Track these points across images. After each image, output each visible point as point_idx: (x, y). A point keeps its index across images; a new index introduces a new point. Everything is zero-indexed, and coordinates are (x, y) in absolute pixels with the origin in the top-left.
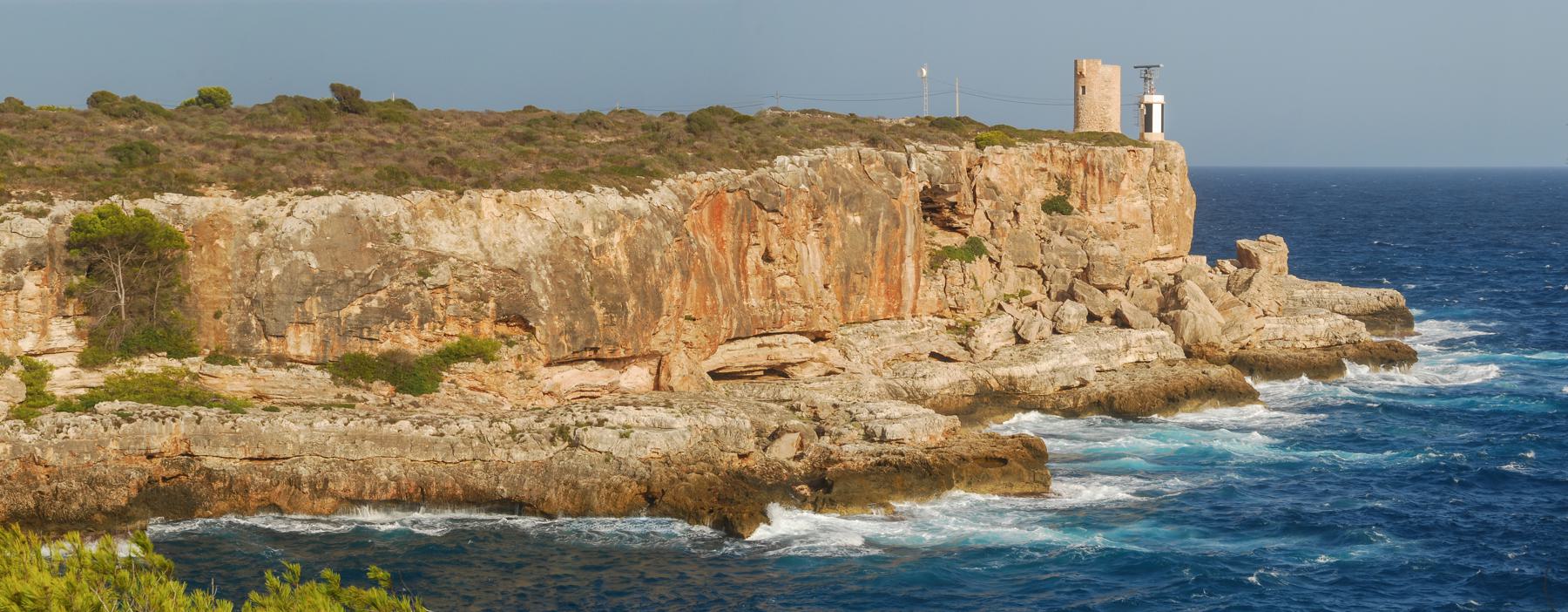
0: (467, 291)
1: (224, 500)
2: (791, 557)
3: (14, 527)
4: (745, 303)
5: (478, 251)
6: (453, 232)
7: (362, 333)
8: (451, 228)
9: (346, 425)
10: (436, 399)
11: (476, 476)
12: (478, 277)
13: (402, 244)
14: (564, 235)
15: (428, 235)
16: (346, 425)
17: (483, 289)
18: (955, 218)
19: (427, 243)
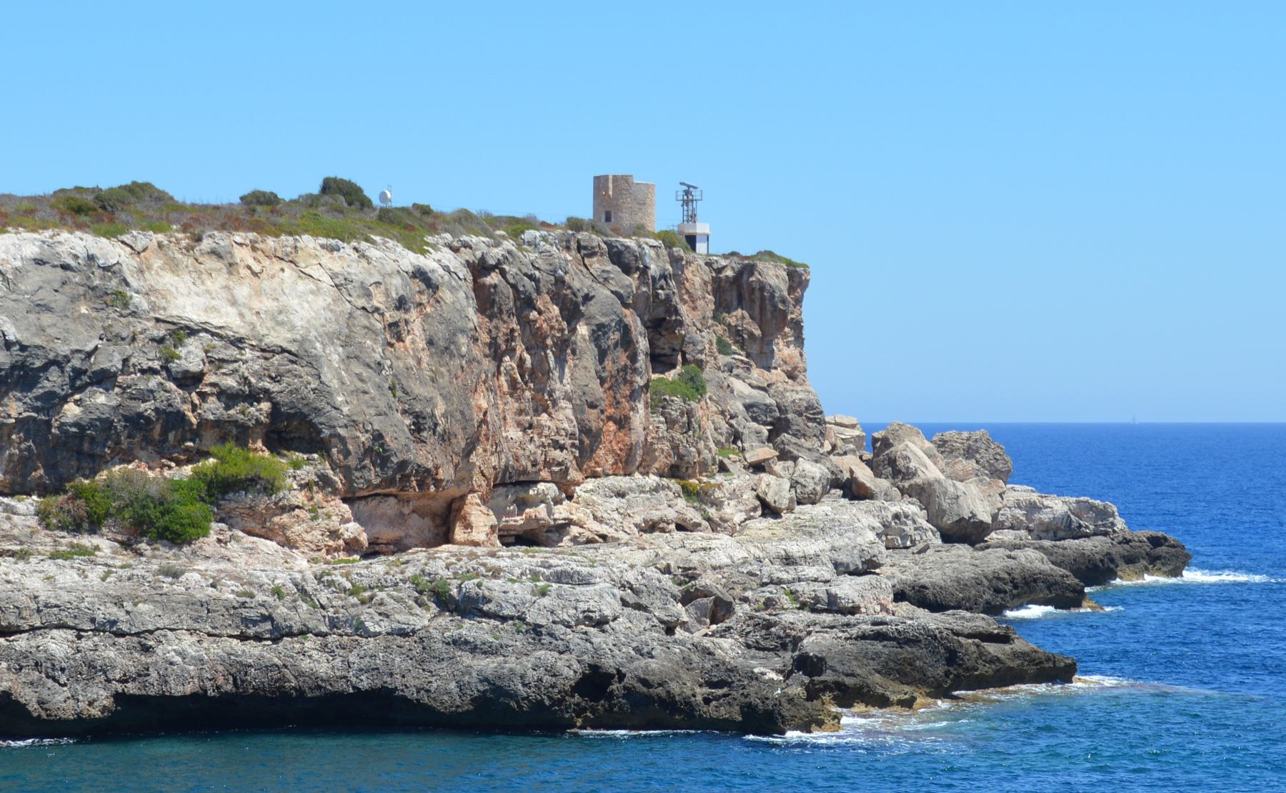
0: (231, 382)
1: (737, 454)
2: (979, 688)
3: (156, 362)
4: (504, 435)
5: (238, 322)
6: (197, 294)
7: (81, 444)
8: (193, 287)
9: (103, 579)
10: (206, 547)
11: (310, 657)
12: (245, 362)
13: (132, 308)
14: (348, 305)
15: (164, 297)
16: (103, 579)
17: (253, 380)
18: (558, 381)
19: (165, 309)
